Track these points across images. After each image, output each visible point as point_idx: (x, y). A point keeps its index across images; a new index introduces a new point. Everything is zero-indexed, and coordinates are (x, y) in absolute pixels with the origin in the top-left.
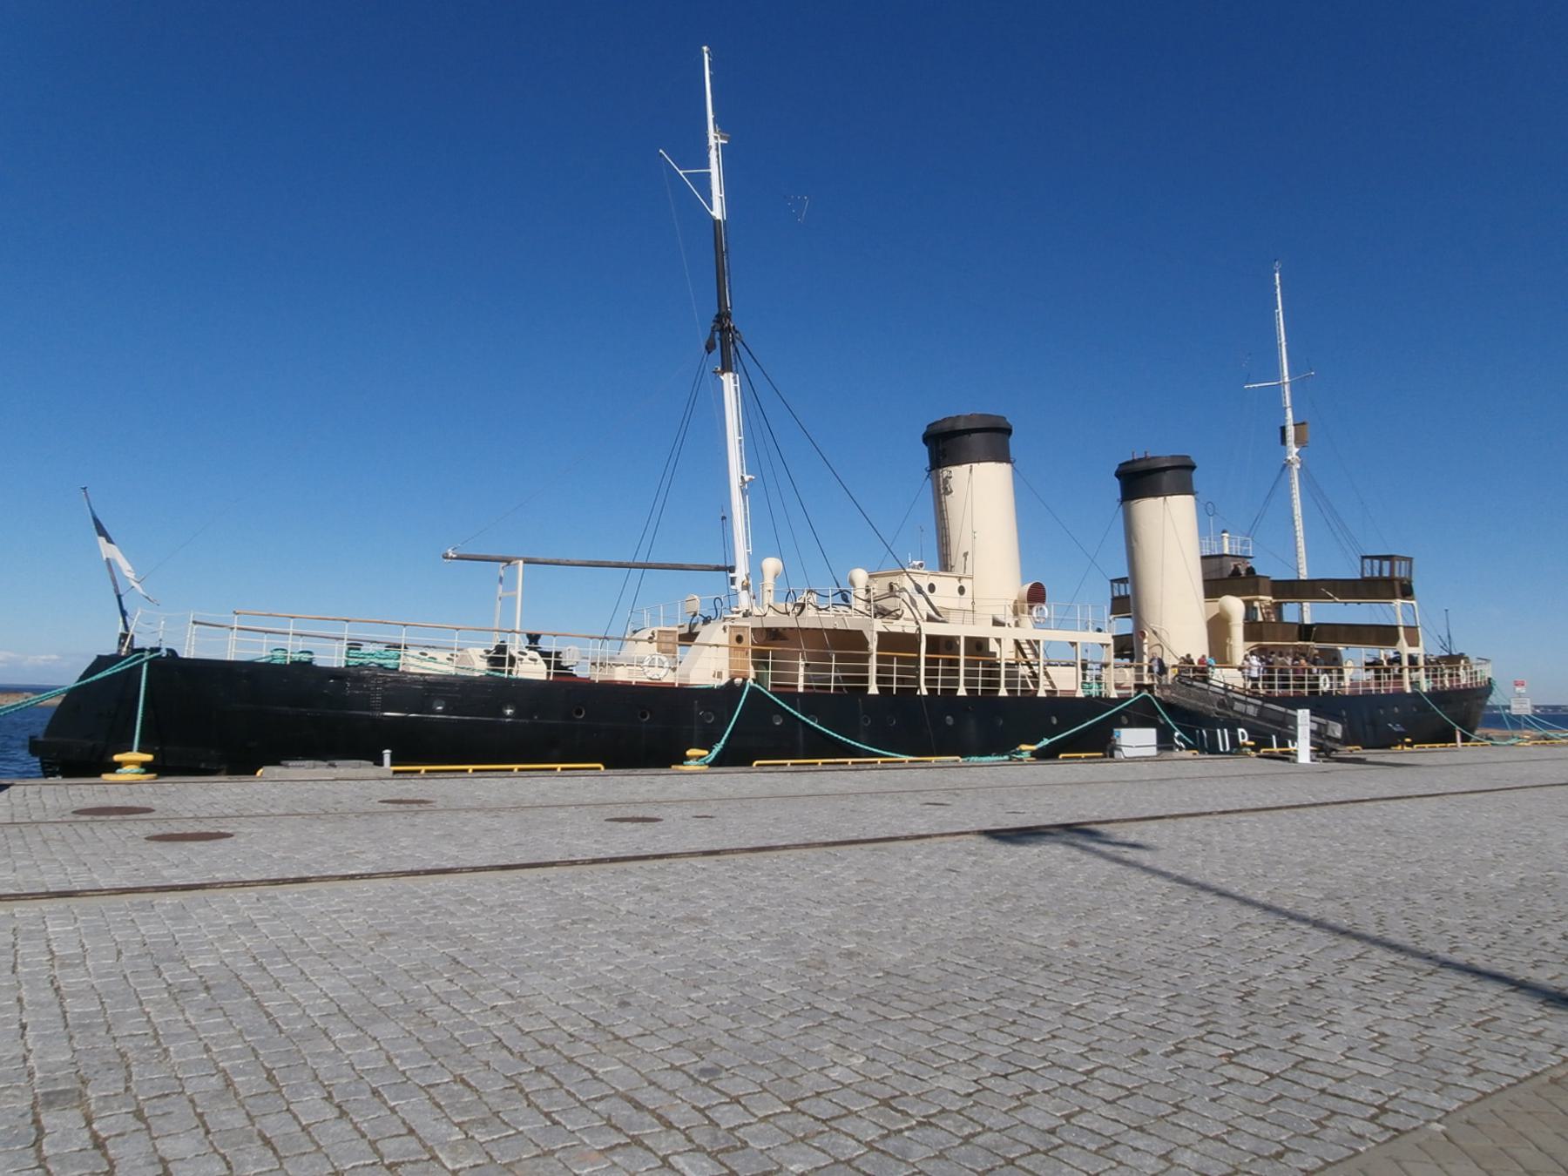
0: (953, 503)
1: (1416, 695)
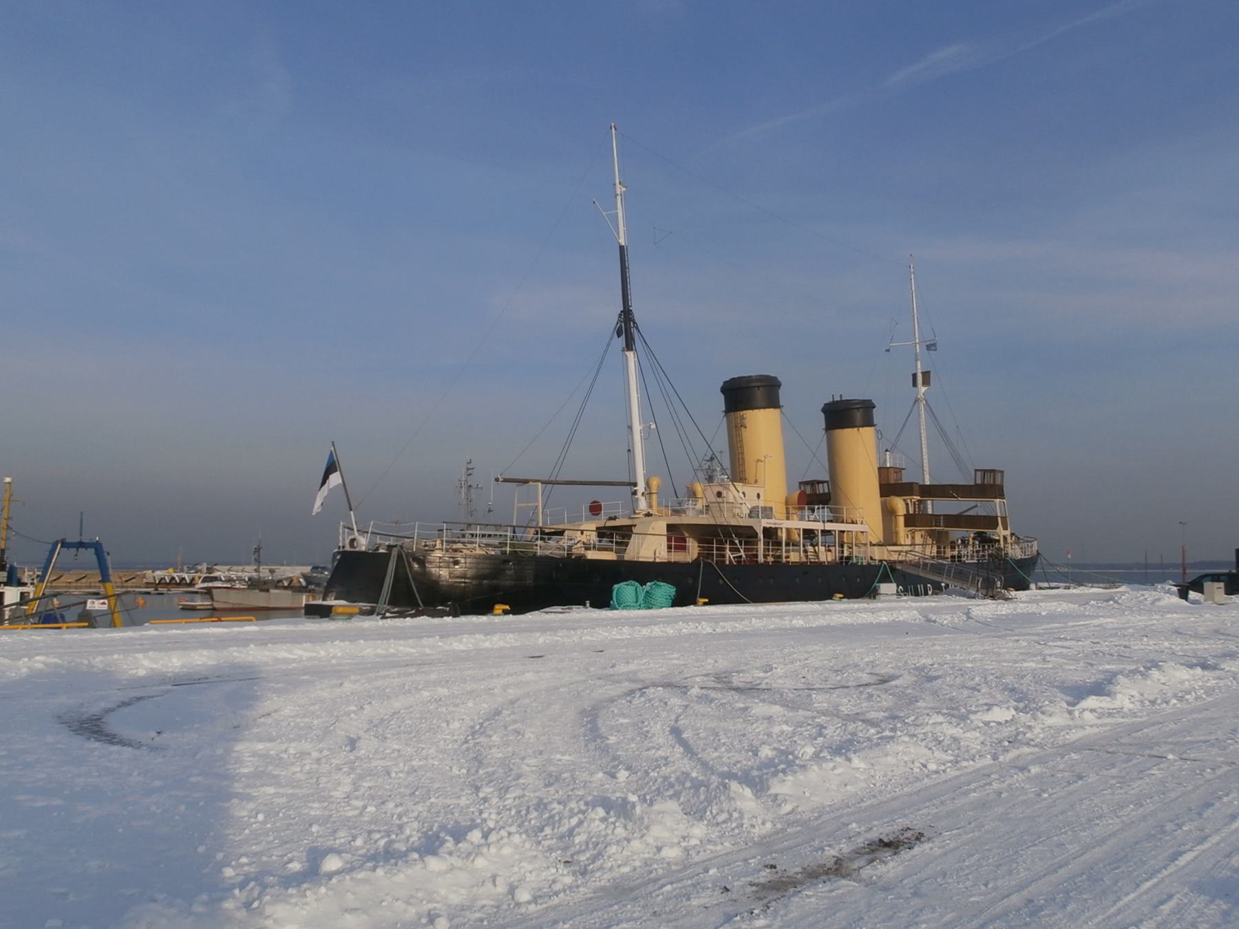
0: (746, 433)
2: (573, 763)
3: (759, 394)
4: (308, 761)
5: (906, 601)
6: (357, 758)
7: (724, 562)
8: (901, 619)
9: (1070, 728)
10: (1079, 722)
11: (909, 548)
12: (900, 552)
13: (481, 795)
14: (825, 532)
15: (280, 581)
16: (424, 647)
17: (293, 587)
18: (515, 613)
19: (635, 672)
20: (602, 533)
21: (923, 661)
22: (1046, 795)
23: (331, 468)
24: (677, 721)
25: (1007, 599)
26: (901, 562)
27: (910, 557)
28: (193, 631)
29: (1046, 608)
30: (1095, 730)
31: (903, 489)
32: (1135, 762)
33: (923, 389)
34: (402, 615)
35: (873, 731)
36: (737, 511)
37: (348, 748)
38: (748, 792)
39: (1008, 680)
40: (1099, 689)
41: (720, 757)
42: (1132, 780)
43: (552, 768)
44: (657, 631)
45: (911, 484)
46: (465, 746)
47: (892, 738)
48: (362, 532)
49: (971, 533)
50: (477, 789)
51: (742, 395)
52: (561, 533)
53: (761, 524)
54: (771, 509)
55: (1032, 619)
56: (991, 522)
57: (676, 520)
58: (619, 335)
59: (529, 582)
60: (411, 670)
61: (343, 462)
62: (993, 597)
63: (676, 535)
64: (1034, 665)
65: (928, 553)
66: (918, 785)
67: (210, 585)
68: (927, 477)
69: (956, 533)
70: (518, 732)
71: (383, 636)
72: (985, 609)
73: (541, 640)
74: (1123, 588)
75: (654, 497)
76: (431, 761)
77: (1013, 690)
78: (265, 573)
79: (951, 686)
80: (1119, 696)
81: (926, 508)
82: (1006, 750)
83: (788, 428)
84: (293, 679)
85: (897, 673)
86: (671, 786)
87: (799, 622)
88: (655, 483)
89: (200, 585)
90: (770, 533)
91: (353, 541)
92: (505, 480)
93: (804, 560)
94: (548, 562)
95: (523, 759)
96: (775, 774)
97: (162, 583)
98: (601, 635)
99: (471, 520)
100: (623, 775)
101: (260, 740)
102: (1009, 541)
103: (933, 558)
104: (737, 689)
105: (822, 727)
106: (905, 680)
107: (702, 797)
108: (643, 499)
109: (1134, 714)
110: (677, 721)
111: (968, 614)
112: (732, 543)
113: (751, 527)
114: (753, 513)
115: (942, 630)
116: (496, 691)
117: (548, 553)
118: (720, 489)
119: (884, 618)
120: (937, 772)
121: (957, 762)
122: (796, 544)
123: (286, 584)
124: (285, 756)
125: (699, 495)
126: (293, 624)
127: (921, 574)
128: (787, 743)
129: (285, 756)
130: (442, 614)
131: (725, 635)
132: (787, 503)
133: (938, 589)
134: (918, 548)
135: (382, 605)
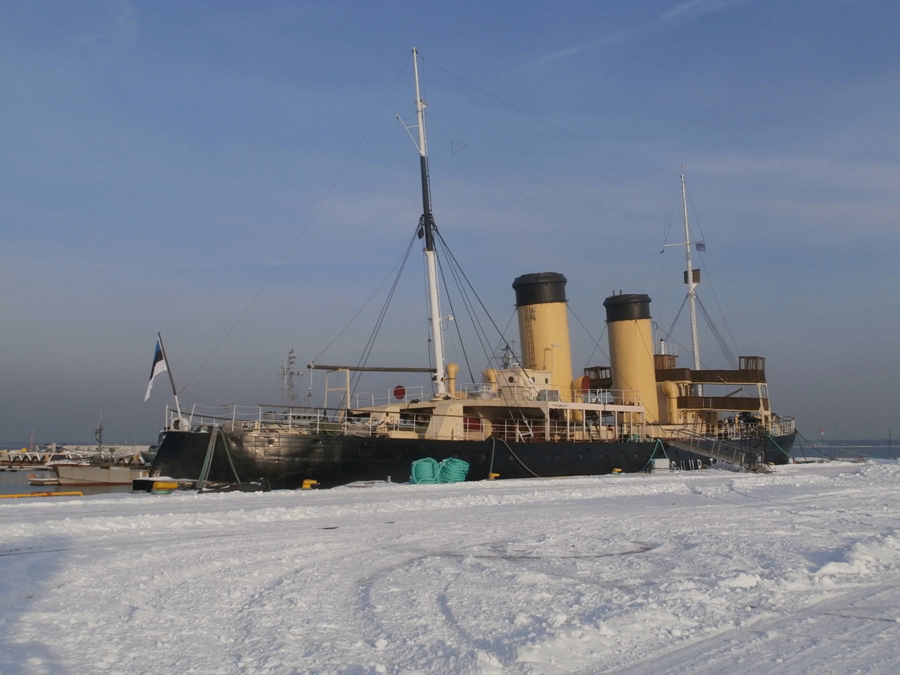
0: (536, 326)
1: (639, 442)
2: (338, 631)
3: (547, 290)
4: (84, 631)
5: (677, 475)
6: (131, 628)
7: (514, 440)
8: (670, 491)
9: (809, 593)
10: (819, 587)
11: (682, 427)
12: (672, 431)
13: (241, 665)
14: (606, 413)
15: (121, 459)
16: (229, 519)
17: (133, 465)
18: (321, 487)
19: (417, 543)
20: (404, 414)
21: (684, 530)
22: (780, 661)
23: (159, 356)
24: (446, 589)
25: (767, 472)
26: (673, 440)
27: (682, 435)
28: (21, 505)
29: (800, 480)
30: (832, 595)
31: (675, 374)
32: (867, 625)
33: (694, 285)
34: (217, 490)
35: (626, 598)
36: (526, 394)
37: (126, 618)
38: (494, 661)
39: (759, 547)
40: (839, 556)
41: (478, 625)
42: (862, 644)
43: (316, 638)
44: (447, 503)
45: (683, 370)
46: (239, 615)
47: (641, 605)
48: (186, 414)
49: (737, 414)
50: (239, 658)
51: (532, 290)
52: (367, 415)
53: (547, 406)
54: (557, 392)
55: (787, 490)
56: (754, 403)
57: (471, 403)
58: (420, 236)
59: (337, 459)
60: (212, 541)
61: (168, 351)
62: (755, 471)
63: (472, 415)
64: (783, 533)
65: (698, 432)
66: (662, 651)
67: (56, 462)
68: (697, 363)
69: (724, 414)
70: (291, 601)
71: (194, 509)
72: (746, 481)
73: (339, 513)
74: (871, 461)
75: (453, 382)
76: (200, 631)
77: (762, 557)
78: (105, 453)
79: (707, 553)
80: (856, 562)
81: (696, 392)
82: (748, 616)
83: (574, 321)
84: (97, 550)
85: (659, 541)
86: (425, 654)
87: (577, 495)
88: (453, 369)
89: (49, 463)
90: (557, 414)
91: (177, 422)
92: (317, 367)
93: (587, 437)
94: (355, 440)
95: (289, 628)
96: (523, 643)
97: (16, 461)
98: (396, 507)
99: (293, 404)
100: (381, 644)
101: (46, 610)
102: (770, 420)
103: (702, 436)
104: (510, 558)
105: (581, 594)
106: (667, 547)
107: (452, 666)
108: (442, 383)
109: (869, 578)
110: (446, 589)
111: (731, 487)
112: (522, 423)
113: (539, 409)
114: (541, 396)
115: (706, 500)
116: (284, 561)
117: (354, 432)
118: (512, 375)
119: (655, 490)
120: (681, 638)
121: (701, 628)
122: (579, 424)
123: (127, 462)
124: (64, 626)
125: (493, 380)
126: (115, 498)
127: (692, 450)
128: (544, 610)
129: (64, 626)
130: (254, 489)
131: (509, 507)
132: (572, 387)
133: (707, 464)
134: (690, 427)
135: (203, 480)
